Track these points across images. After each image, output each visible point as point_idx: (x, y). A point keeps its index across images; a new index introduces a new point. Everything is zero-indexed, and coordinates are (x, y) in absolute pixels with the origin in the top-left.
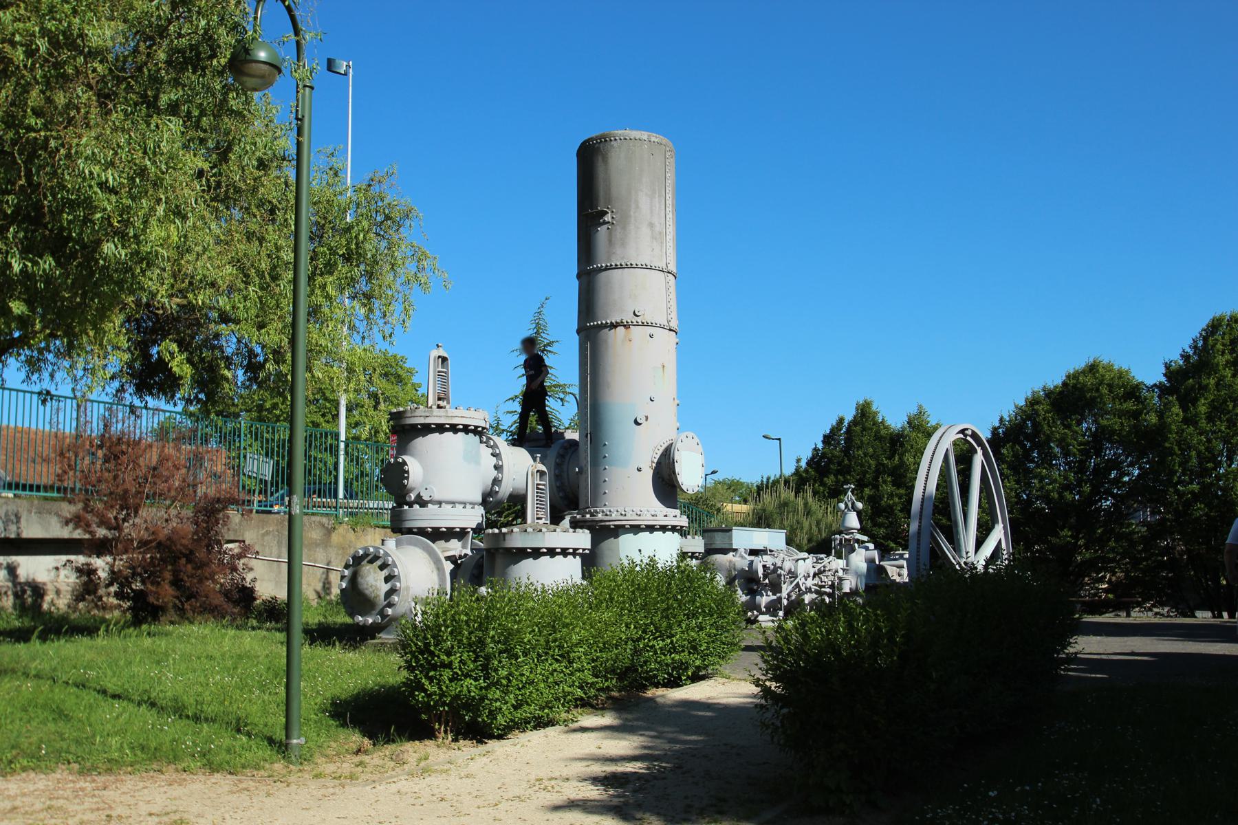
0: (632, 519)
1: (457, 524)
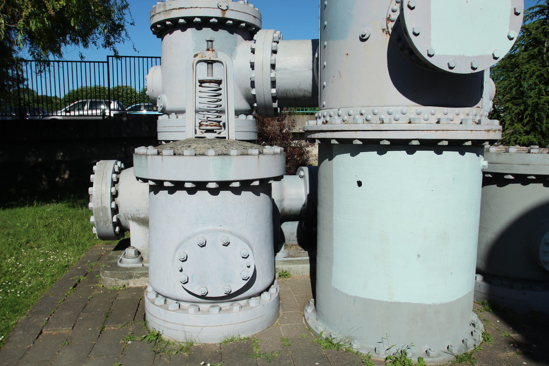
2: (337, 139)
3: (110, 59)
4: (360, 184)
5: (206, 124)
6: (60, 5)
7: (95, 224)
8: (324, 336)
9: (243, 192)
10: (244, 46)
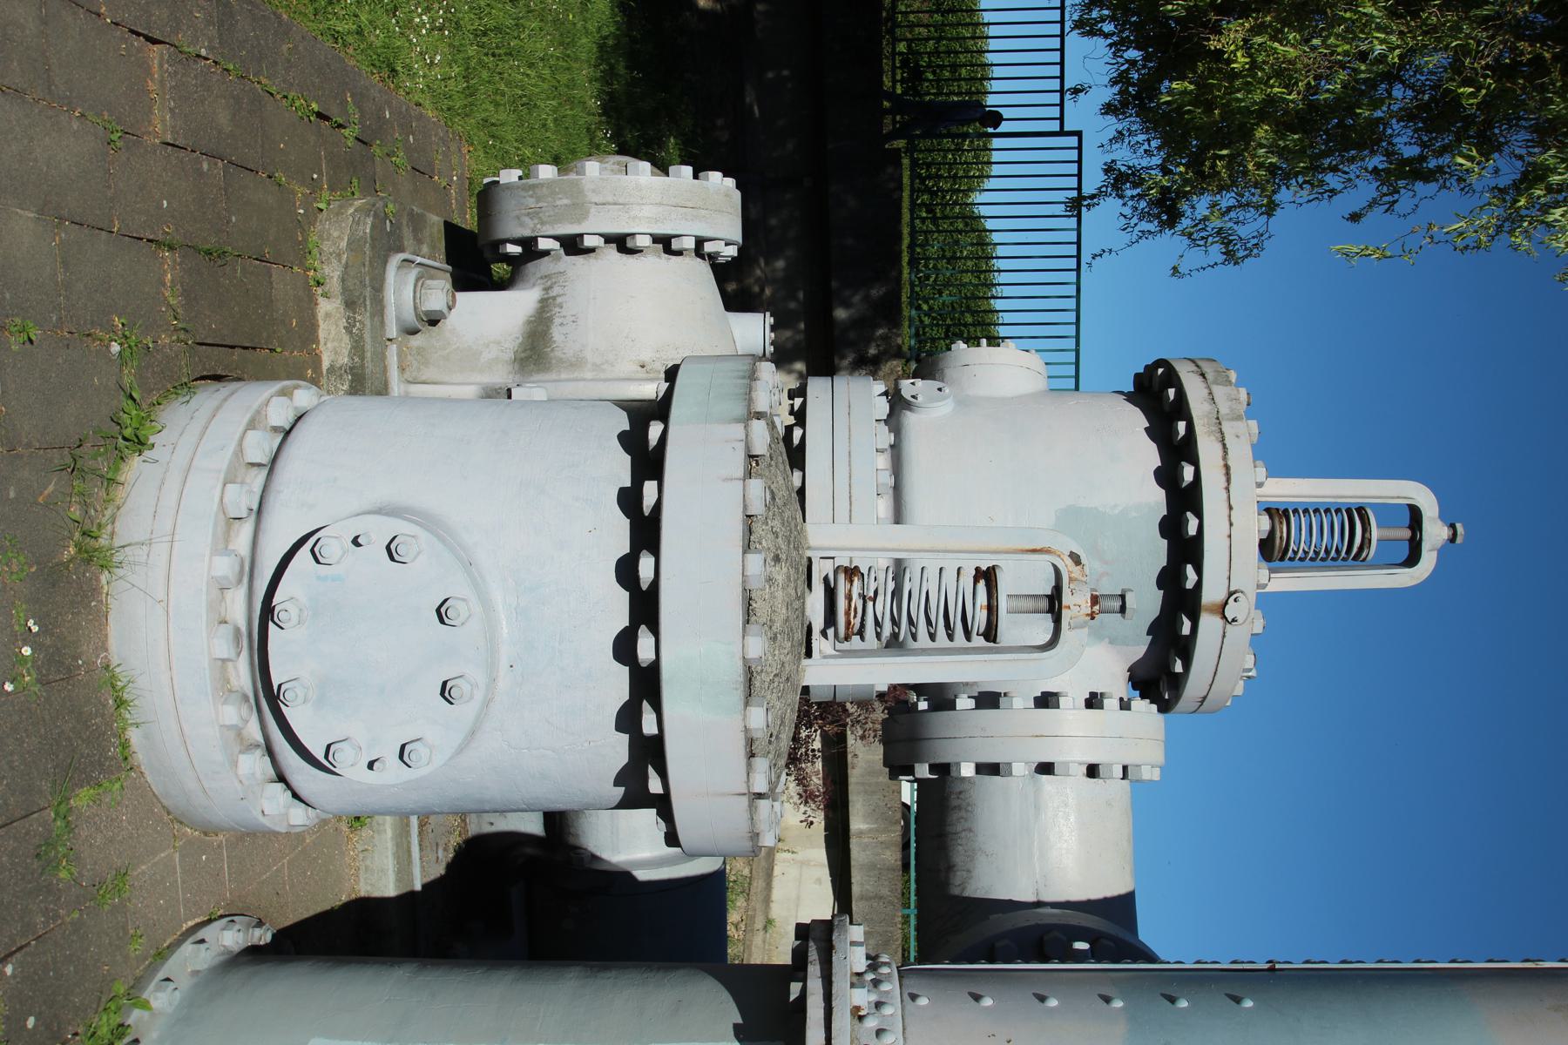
3: (1073, 141)
5: (855, 596)
6: (1234, 52)
7: (531, 181)
8: (135, 1017)
9: (626, 737)
10: (1113, 679)
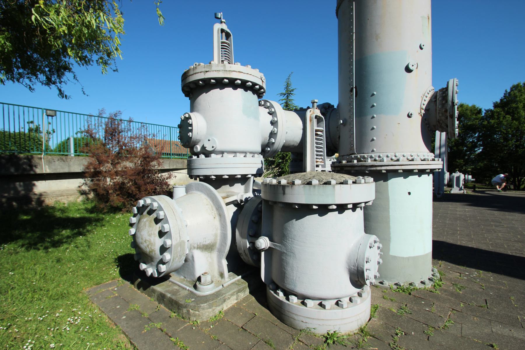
0: (404, 164)
1: (238, 172)
2: (403, 170)
4: (409, 193)
